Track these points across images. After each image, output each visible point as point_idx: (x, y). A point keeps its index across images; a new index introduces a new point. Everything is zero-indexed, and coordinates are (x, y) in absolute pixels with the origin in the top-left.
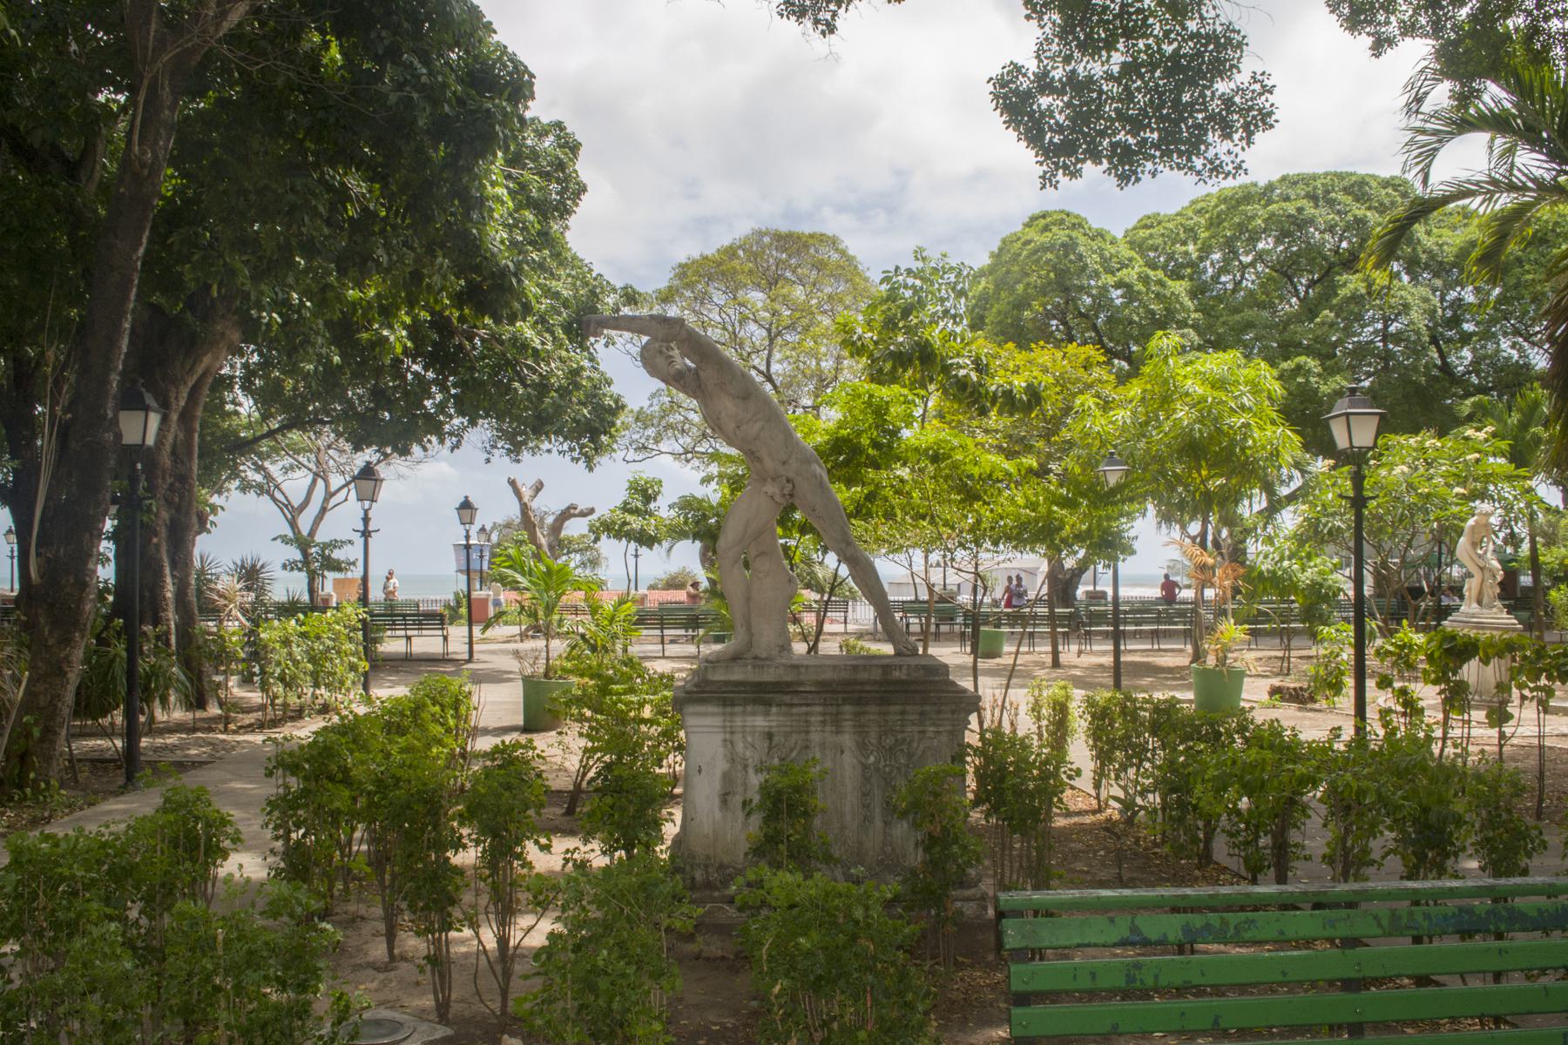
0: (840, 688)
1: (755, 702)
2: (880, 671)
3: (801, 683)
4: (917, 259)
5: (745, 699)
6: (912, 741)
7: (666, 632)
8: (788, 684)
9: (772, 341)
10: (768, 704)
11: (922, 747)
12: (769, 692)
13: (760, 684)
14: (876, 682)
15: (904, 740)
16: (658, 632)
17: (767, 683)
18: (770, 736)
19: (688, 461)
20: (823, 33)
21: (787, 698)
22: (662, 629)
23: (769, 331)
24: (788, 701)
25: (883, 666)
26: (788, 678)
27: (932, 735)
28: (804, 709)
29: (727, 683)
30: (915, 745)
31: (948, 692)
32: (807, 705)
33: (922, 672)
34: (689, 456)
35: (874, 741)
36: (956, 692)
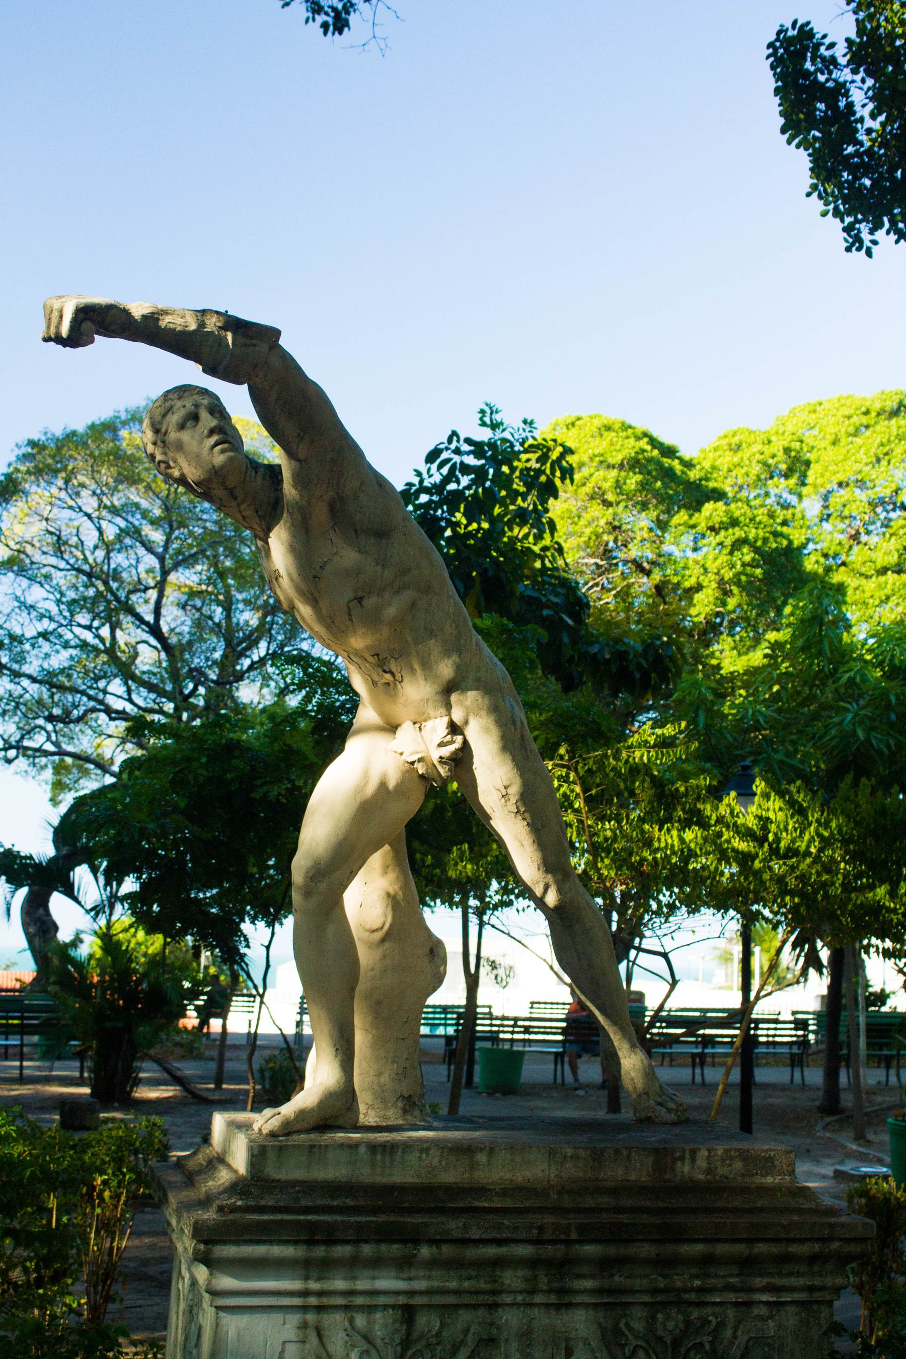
0: (567, 1202)
1: (384, 1235)
2: (650, 1161)
3: (481, 1191)
4: (483, 424)
5: (360, 1227)
6: (721, 1325)
7: (25, 1063)
8: (453, 1191)
9: (165, 573)
10: (413, 1238)
11: (742, 1339)
12: (411, 1211)
13: (389, 1190)
14: (641, 1190)
15: (705, 1322)
16: (17, 1063)
17: (402, 1189)
18: (408, 1313)
19: (9, 761)
20: (325, 26)
21: (454, 1226)
22: (21, 1060)
23: (161, 559)
24: (456, 1235)
25: (656, 1151)
26: (448, 1177)
27: (763, 1311)
28: (491, 1251)
29: (310, 1187)
30: (728, 1333)
31: (799, 1211)
32: (499, 1242)
33: (738, 1165)
34: (12, 753)
35: (639, 1326)
36: (816, 1211)
